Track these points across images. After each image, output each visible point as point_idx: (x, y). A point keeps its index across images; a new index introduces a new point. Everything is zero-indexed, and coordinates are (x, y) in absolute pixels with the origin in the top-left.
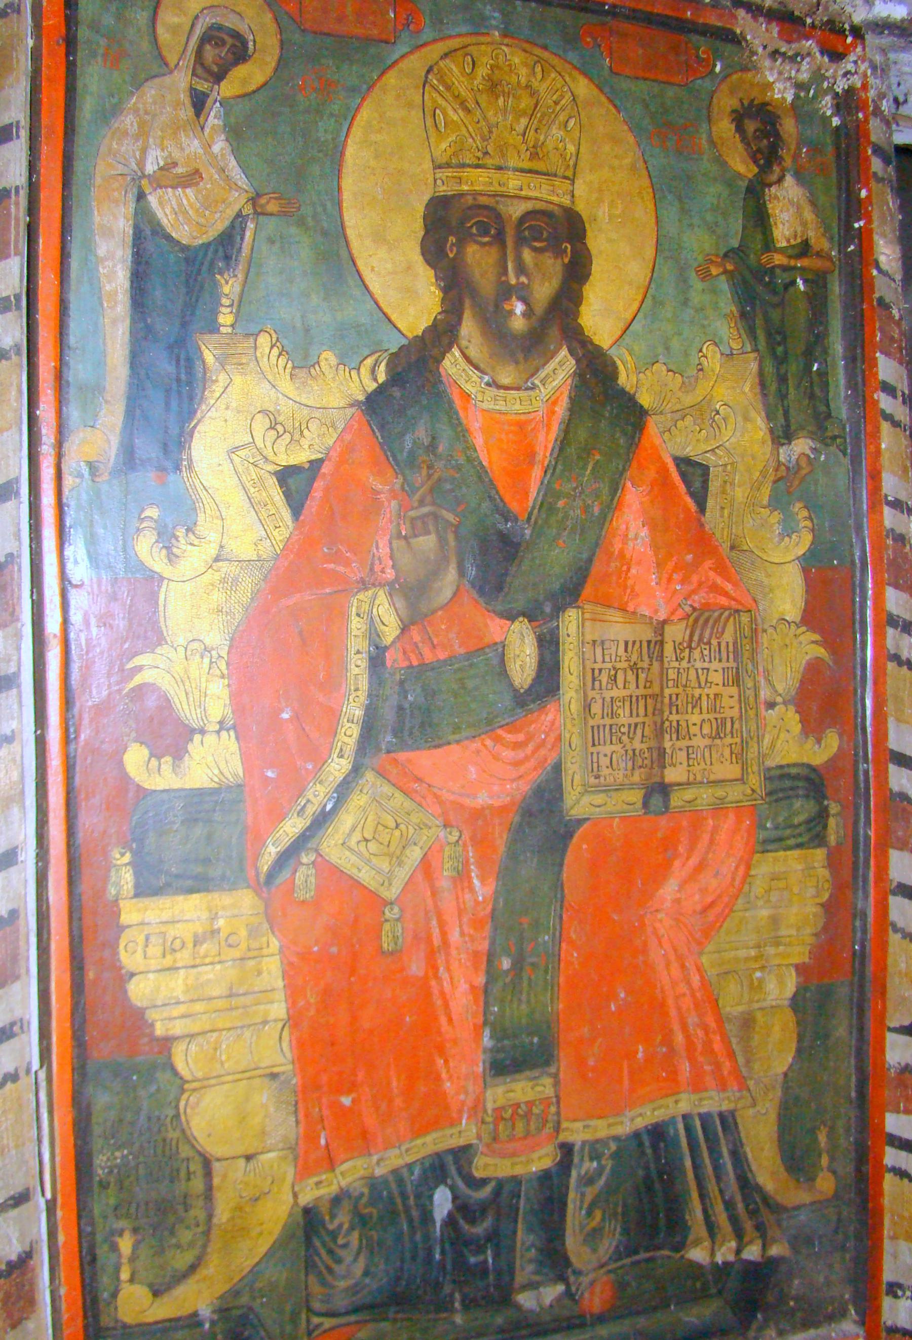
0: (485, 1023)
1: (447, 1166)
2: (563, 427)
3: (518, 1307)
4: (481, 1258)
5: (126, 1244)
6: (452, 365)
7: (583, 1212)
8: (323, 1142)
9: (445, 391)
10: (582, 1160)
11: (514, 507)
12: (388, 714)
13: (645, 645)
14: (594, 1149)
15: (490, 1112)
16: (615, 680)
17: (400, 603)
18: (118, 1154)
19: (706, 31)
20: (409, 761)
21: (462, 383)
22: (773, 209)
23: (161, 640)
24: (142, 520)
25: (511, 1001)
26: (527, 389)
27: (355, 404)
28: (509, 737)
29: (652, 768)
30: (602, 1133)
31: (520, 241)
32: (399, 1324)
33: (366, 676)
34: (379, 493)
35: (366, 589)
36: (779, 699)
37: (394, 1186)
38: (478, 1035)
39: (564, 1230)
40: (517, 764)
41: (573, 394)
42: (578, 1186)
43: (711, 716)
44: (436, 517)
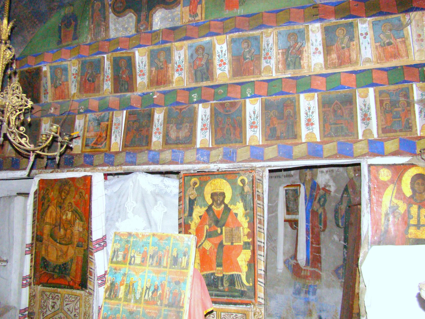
1: (213, 274)
6: (213, 206)
14: (226, 275)
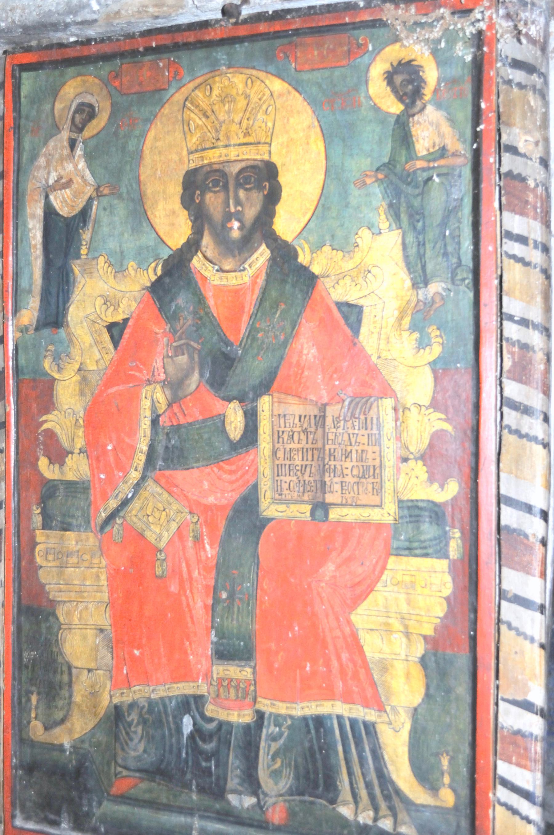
0: (212, 627)
2: (262, 291)
3: (229, 803)
4: (208, 764)
5: (34, 699)
6: (197, 262)
7: (270, 757)
8: (125, 672)
9: (193, 277)
10: (269, 724)
11: (232, 338)
12: (160, 449)
13: (312, 418)
14: (278, 720)
15: (215, 679)
16: (293, 438)
17: (168, 392)
18: (32, 653)
19: (365, 25)
20: (171, 475)
21: (203, 272)
22: (416, 131)
23: (54, 409)
24: (47, 351)
25: (227, 618)
26: (240, 271)
27: (147, 288)
28: (227, 467)
29: (316, 493)
30: (283, 711)
31: (239, 185)
32: (161, 787)
33: (150, 429)
34: (156, 333)
35: (150, 384)
36: (411, 456)
37: (161, 707)
38: (208, 634)
39: (257, 764)
40: (232, 482)
41: (268, 271)
42: (266, 740)
43: (360, 464)
44: (188, 345)
